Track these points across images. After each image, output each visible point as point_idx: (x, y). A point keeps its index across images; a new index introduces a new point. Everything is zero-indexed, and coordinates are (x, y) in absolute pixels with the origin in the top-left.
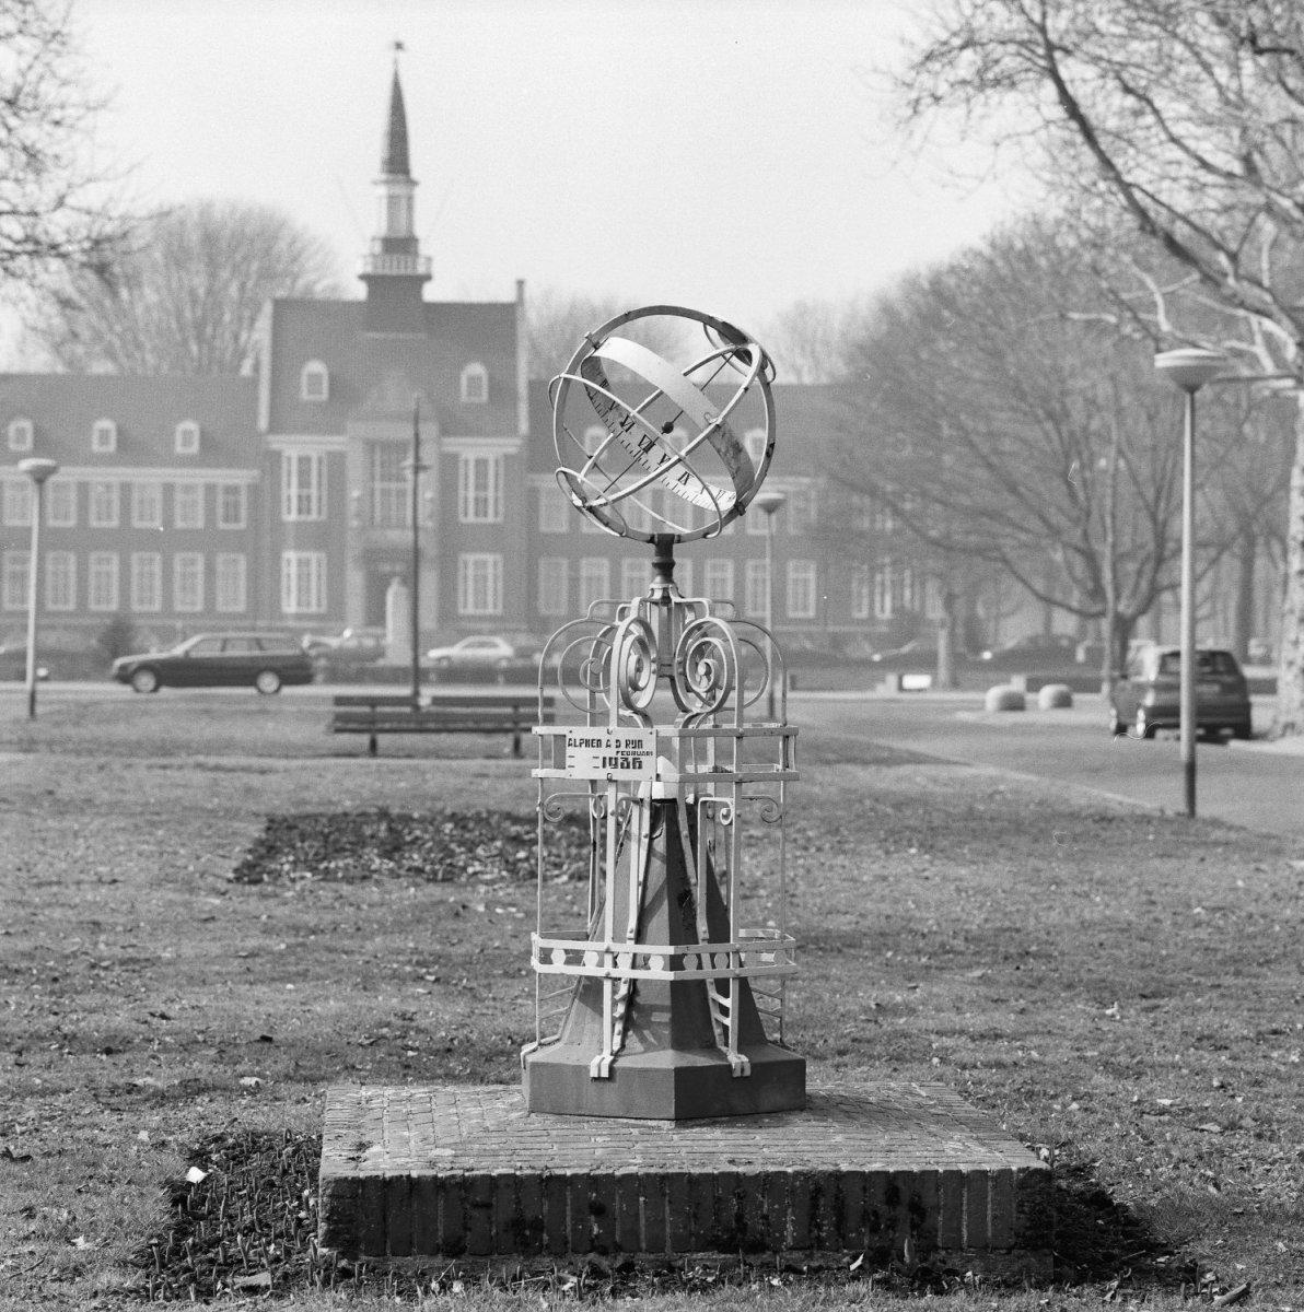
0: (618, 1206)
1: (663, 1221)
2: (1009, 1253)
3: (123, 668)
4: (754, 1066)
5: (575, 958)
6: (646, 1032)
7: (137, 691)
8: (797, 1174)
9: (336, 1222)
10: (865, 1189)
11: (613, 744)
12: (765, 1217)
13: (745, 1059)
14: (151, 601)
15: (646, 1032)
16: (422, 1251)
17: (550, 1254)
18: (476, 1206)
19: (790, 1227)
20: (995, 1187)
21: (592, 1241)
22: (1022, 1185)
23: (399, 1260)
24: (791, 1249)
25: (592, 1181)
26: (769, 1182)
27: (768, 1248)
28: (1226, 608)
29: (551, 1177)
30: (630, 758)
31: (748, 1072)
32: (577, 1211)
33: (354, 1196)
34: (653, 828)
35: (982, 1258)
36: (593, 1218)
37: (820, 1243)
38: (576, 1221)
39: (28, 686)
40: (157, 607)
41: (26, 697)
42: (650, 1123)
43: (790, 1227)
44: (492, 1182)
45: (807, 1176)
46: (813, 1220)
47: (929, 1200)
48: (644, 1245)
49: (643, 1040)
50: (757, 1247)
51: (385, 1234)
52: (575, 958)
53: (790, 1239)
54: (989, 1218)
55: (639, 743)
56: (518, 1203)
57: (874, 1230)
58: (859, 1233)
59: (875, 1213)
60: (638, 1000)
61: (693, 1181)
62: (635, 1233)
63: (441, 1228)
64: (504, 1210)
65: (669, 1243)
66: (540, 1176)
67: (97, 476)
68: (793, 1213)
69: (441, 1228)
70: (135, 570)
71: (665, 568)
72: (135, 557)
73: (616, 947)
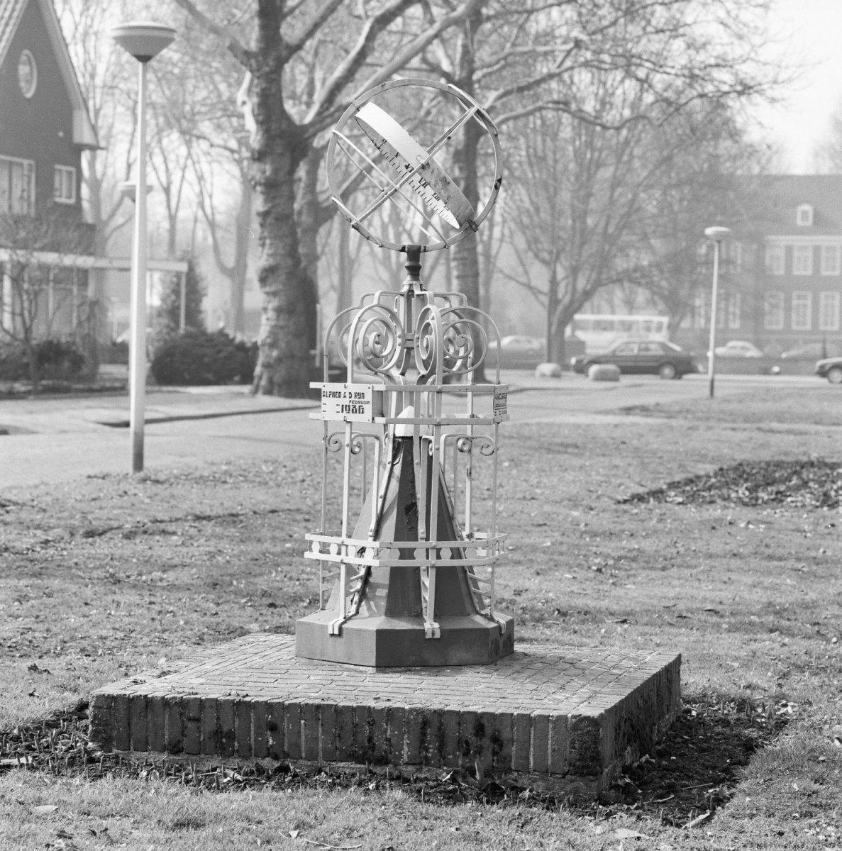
0: (287, 726)
1: (317, 738)
2: (564, 777)
3: (822, 367)
4: (442, 632)
5: (324, 549)
6: (372, 603)
7: (831, 382)
8: (411, 710)
9: (97, 725)
10: (459, 724)
11: (348, 395)
12: (388, 740)
13: (436, 625)
14: (804, 324)
15: (372, 603)
16: (154, 749)
17: (239, 756)
18: (190, 719)
19: (406, 748)
20: (554, 728)
21: (268, 749)
22: (575, 728)
23: (139, 754)
24: (407, 764)
25: (269, 706)
26: (391, 714)
27: (390, 762)
28: (708, 305)
29: (239, 702)
30: (357, 406)
31: (438, 635)
32: (258, 727)
33: (109, 708)
34: (394, 457)
35: (543, 779)
36: (269, 733)
37: (427, 761)
38: (258, 734)
39: (709, 376)
40: (808, 327)
41: (708, 384)
42: (361, 668)
43: (406, 748)
44: (202, 704)
45: (419, 712)
46: (422, 744)
47: (506, 735)
48: (303, 755)
49: (369, 608)
50: (383, 761)
51: (129, 736)
52: (324, 549)
53: (405, 757)
54: (549, 751)
55: (361, 395)
56: (218, 719)
57: (466, 754)
58: (455, 756)
59: (467, 743)
60: (371, 580)
61: (338, 711)
62: (298, 746)
63: (167, 733)
64: (209, 724)
65: (321, 754)
66: (233, 701)
67: (797, 241)
68: (408, 738)
69: (167, 733)
70: (822, 302)
71: (415, 271)
72: (823, 295)
73: (347, 541)
